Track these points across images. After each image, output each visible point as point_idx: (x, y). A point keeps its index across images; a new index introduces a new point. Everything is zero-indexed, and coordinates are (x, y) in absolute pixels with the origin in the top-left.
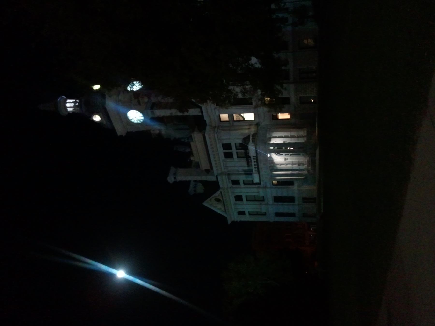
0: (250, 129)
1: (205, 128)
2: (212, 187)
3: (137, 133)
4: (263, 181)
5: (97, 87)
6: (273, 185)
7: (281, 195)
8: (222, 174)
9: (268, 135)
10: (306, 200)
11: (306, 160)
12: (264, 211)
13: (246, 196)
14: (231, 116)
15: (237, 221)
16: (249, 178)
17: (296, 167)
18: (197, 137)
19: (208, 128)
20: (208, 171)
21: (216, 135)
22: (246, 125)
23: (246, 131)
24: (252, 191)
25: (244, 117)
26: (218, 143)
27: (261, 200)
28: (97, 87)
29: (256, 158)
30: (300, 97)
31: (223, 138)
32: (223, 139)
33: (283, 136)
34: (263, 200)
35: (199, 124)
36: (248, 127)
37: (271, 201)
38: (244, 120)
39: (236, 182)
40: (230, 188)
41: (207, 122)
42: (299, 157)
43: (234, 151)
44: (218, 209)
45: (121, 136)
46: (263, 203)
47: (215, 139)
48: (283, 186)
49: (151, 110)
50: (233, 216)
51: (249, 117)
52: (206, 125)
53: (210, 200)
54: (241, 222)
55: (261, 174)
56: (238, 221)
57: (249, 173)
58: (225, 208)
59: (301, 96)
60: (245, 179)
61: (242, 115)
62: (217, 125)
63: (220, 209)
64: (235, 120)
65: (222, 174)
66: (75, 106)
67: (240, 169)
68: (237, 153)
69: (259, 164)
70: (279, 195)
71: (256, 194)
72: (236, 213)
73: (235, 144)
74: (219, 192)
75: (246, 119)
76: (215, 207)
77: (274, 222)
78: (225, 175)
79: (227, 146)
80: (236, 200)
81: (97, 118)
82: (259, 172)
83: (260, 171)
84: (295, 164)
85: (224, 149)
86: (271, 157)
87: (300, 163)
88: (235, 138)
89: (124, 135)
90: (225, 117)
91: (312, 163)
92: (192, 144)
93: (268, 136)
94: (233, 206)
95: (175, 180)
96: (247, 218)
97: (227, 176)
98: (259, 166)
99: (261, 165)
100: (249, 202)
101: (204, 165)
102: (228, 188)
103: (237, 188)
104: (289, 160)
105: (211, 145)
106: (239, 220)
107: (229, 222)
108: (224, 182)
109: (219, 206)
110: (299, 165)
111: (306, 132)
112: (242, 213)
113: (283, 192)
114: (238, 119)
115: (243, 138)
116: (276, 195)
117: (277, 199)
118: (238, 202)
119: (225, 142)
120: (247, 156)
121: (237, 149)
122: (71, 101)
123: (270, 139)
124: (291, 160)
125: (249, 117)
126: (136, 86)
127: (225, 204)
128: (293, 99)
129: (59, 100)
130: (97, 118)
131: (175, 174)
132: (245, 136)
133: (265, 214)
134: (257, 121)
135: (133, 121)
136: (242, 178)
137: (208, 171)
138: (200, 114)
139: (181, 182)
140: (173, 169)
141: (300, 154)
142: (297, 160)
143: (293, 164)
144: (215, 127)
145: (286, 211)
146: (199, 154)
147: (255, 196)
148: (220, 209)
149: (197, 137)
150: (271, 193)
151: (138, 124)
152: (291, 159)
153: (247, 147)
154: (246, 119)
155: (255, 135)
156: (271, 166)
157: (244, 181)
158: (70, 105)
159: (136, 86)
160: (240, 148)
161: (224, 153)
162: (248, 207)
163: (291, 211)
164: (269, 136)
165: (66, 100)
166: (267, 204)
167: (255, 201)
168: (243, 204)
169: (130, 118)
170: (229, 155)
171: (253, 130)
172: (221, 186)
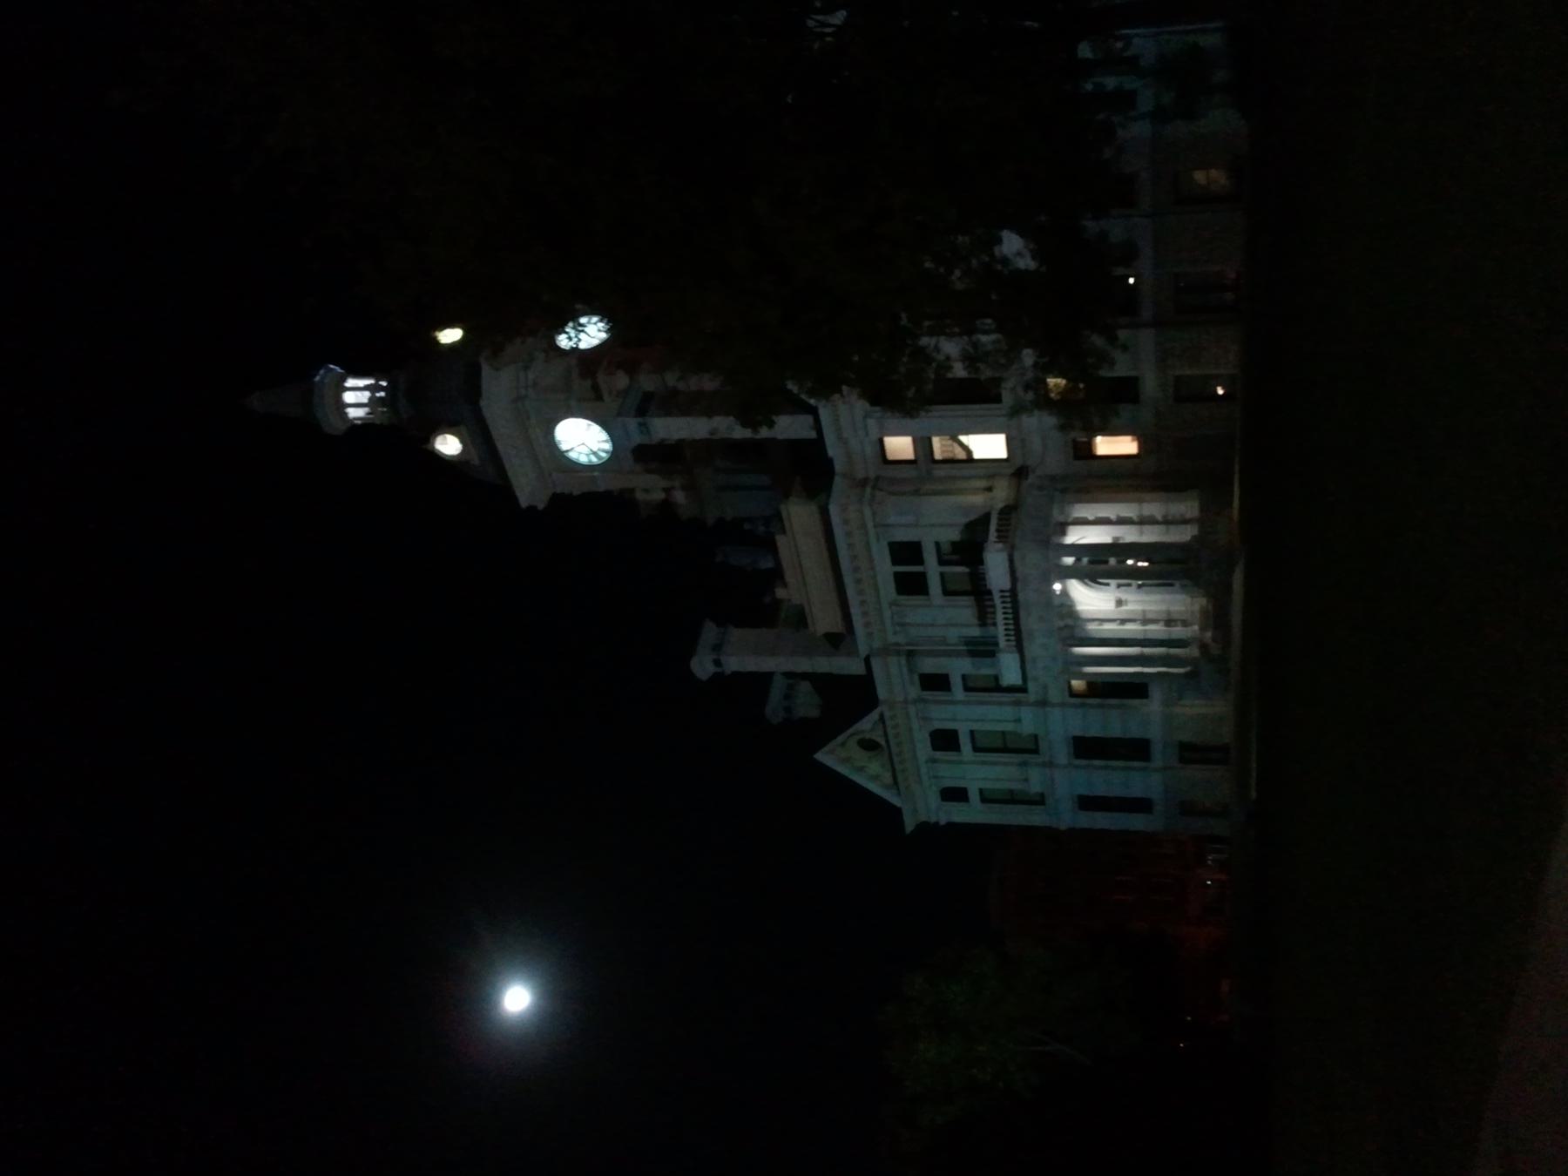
2: (851, 698)
3: (584, 502)
5: (450, 336)
9: (1055, 512)
10: (1190, 753)
11: (1197, 607)
12: (1035, 787)
13: (972, 732)
14: (923, 445)
15: (937, 823)
18: (799, 514)
19: (837, 480)
20: (838, 641)
21: (867, 512)
23: (978, 499)
24: (994, 716)
25: (972, 447)
26: (873, 540)
28: (450, 336)
31: (892, 520)
33: (1113, 517)
34: (1036, 751)
35: (809, 469)
36: (983, 484)
37: (1062, 755)
38: (970, 459)
39: (936, 683)
40: (915, 702)
41: (839, 467)
43: (932, 568)
44: (870, 775)
47: (864, 526)
50: (922, 806)
51: (989, 446)
53: (843, 744)
55: (1027, 653)
56: (943, 822)
57: (983, 649)
61: (963, 438)
62: (872, 475)
64: (938, 455)
66: (373, 402)
67: (953, 634)
68: (942, 575)
69: (1023, 621)
71: (1009, 727)
72: (934, 799)
74: (874, 715)
75: (976, 456)
76: (861, 769)
77: (1072, 832)
78: (898, 653)
79: (906, 552)
80: (935, 748)
81: (449, 445)
82: (1020, 648)
85: (895, 562)
86: (1065, 592)
87: (1175, 616)
88: (936, 522)
90: (900, 446)
91: (1217, 618)
92: (781, 541)
96: (972, 813)
97: (903, 661)
99: (1030, 622)
101: (824, 620)
102: (906, 701)
105: (849, 534)
107: (909, 825)
108: (892, 682)
110: (1169, 622)
112: (955, 795)
116: (1078, 733)
117: (1086, 748)
120: (978, 591)
121: (942, 562)
122: (362, 383)
123: (1062, 529)
125: (989, 446)
126: (591, 333)
128: (1150, 385)
129: (317, 378)
130: (449, 445)
131: (717, 648)
132: (973, 517)
134: (1018, 462)
135: (573, 455)
136: (958, 667)
137: (838, 641)
139: (736, 674)
140: (710, 632)
142: (1163, 607)
143: (1146, 621)
144: (863, 483)
145: (1117, 791)
147: (1003, 733)
148: (875, 778)
149: (799, 514)
150: (1062, 725)
151: (590, 468)
155: (1008, 511)
157: (964, 677)
159: (591, 333)
160: (954, 557)
162: (977, 773)
164: (1061, 519)
166: (1050, 764)
169: (564, 447)
170: (911, 585)
171: (1002, 493)
172: (882, 693)
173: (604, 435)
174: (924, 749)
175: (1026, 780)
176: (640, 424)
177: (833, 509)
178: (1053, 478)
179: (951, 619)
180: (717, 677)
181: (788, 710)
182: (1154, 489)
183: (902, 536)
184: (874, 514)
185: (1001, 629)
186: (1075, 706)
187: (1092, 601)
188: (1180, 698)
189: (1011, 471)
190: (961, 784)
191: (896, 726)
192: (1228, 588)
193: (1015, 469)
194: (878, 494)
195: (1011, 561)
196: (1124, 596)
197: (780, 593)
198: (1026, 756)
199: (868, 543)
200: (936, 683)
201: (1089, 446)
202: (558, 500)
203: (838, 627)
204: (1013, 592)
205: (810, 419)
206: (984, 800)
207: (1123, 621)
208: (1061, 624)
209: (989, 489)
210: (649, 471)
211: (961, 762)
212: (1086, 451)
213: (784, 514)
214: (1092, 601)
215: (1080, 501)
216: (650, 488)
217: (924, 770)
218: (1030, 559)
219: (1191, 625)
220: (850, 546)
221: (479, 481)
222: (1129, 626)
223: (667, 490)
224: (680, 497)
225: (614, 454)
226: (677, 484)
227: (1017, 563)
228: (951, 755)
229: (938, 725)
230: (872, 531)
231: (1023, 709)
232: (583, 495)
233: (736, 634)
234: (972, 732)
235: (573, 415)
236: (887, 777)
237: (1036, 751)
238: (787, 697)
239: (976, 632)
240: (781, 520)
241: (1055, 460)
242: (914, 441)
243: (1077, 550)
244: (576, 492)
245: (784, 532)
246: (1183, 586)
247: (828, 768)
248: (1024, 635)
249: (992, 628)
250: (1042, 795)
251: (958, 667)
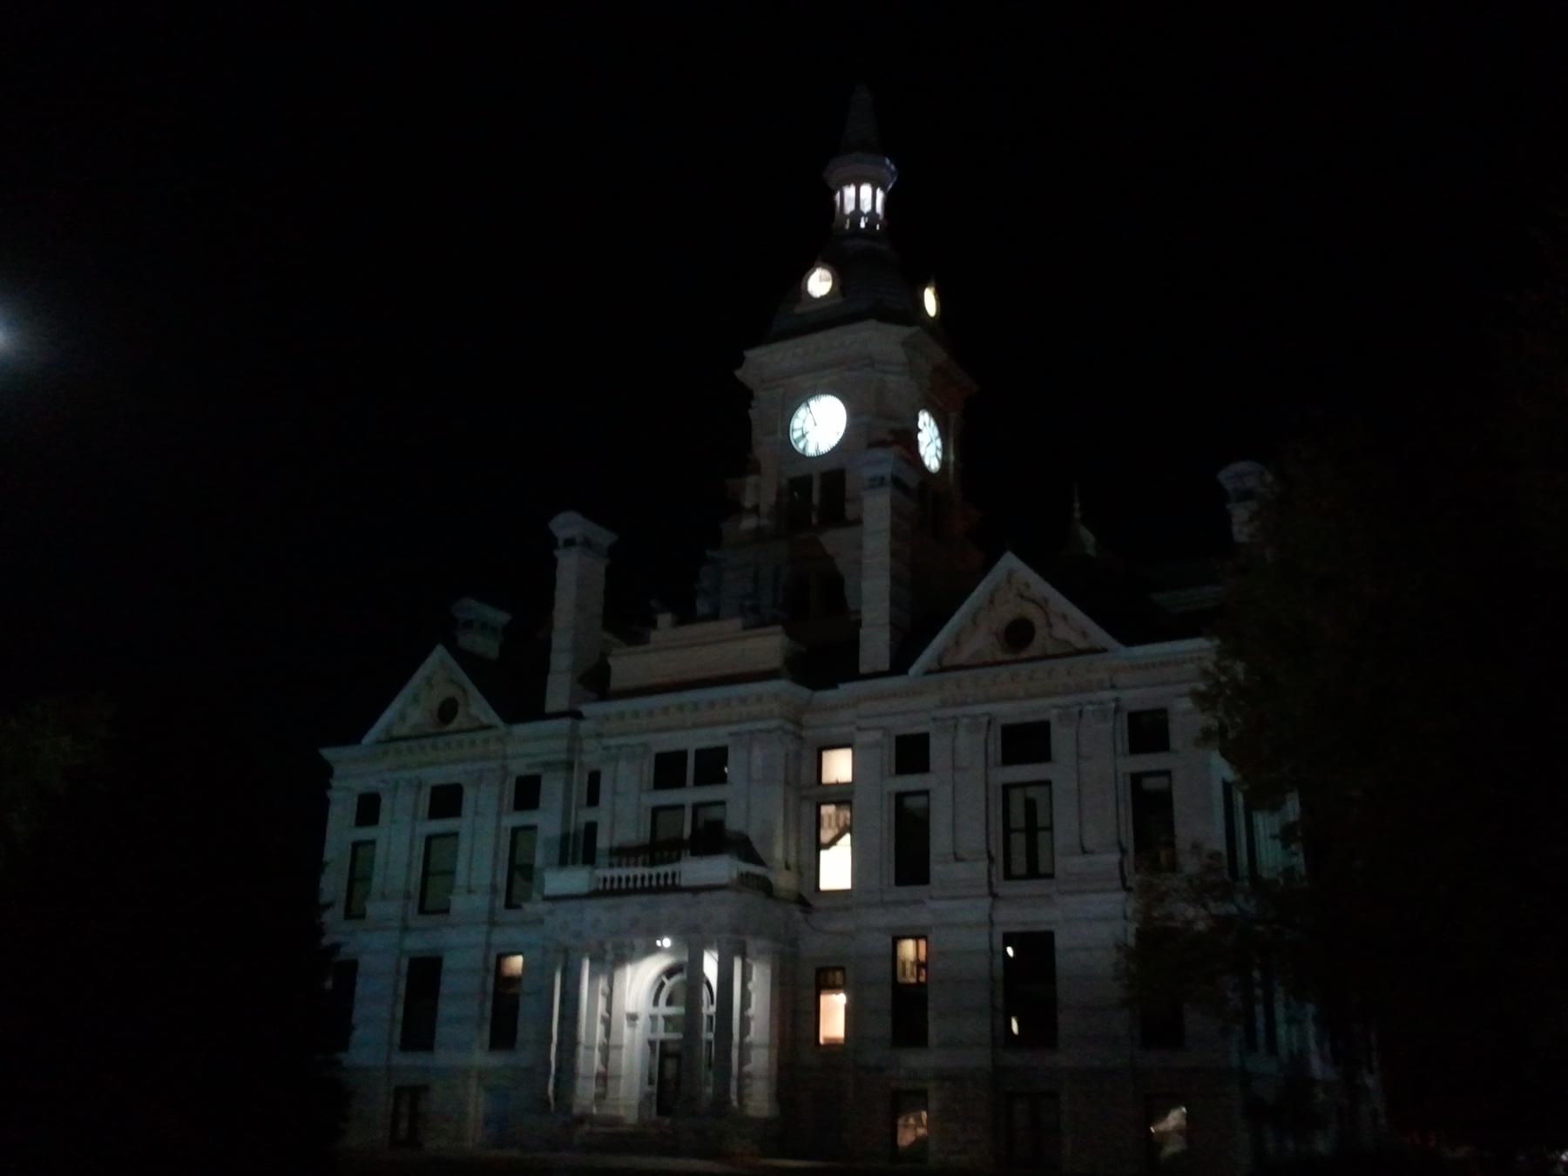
0: (788, 867)
2: (516, 691)
3: (738, 426)
6: (501, 957)
9: (762, 943)
10: (411, 1096)
11: (622, 1112)
14: (841, 795)
17: (589, 1061)
18: (769, 646)
19: (805, 692)
20: (596, 682)
21: (773, 723)
23: (778, 853)
25: (833, 849)
26: (734, 728)
31: (757, 754)
32: (750, 753)
35: (824, 659)
37: (417, 943)
38: (819, 846)
39: (527, 794)
40: (504, 768)
41: (828, 696)
42: (636, 1080)
43: (688, 796)
44: (407, 709)
45: (739, 361)
46: (413, 906)
48: (489, 1004)
49: (888, 478)
50: (352, 771)
51: (836, 869)
54: (324, 804)
55: (592, 902)
57: (579, 847)
58: (406, 738)
61: (847, 839)
63: (402, 717)
65: (574, 737)
67: (601, 815)
68: (681, 807)
69: (634, 899)
71: (461, 878)
72: (361, 786)
73: (722, 803)
75: (823, 853)
76: (416, 699)
78: (570, 750)
79: (712, 766)
80: (436, 790)
81: (819, 283)
82: (594, 894)
84: (605, 1060)
85: (700, 753)
86: (652, 950)
87: (611, 1084)
88: (748, 801)
89: (738, 373)
90: (839, 766)
93: (753, 945)
95: (561, 543)
96: (340, 829)
97: (563, 756)
99: (632, 907)
101: (627, 666)
102: (505, 757)
103: (501, 798)
104: (626, 1030)
105: (621, 715)
106: (333, 795)
107: (328, 753)
108: (531, 743)
110: (603, 1078)
112: (368, 810)
115: (752, 839)
116: (360, 969)
117: (424, 977)
118: (996, 734)
119: (469, 794)
120: (660, 849)
121: (696, 807)
125: (836, 869)
126: (930, 445)
127: (427, 742)
128: (914, 1060)
129: (888, 161)
130: (819, 283)
131: (587, 544)
134: (817, 903)
135: (802, 413)
136: (547, 821)
137: (596, 682)
138: (863, 669)
139: (553, 563)
140: (605, 538)
141: (651, 1082)
142: (624, 1071)
143: (606, 1049)
144: (798, 723)
146: (670, 648)
147: (451, 872)
148: (402, 717)
150: (460, 949)
151: (786, 430)
152: (633, 1044)
155: (765, 887)
157: (533, 828)
159: (930, 445)
160: (701, 824)
161: (683, 755)
162: (398, 842)
165: (884, 189)
166: (406, 929)
168: (499, 814)
169: (812, 403)
170: (668, 770)
171: (784, 881)
172: (522, 729)
173: (825, 448)
175: (470, 891)
176: (882, 479)
179: (625, 814)
180: (551, 542)
181: (469, 624)
184: (769, 731)
185: (608, 873)
186: (486, 960)
190: (384, 817)
191: (486, 741)
192: (674, 1152)
193: (808, 897)
195: (989, 871)
196: (640, 1023)
197: (664, 619)
198: (416, 900)
201: (834, 988)
203: (616, 683)
204: (676, 889)
207: (607, 1023)
208: (609, 947)
209: (788, 867)
210: (779, 494)
211: (415, 817)
213: (770, 629)
214: (639, 983)
217: (407, 774)
218: (721, 910)
220: (636, 714)
221: (776, 310)
223: (756, 510)
224: (748, 523)
225: (802, 457)
226: (765, 522)
232: (746, 425)
233: (600, 567)
234: (455, 834)
238: (484, 625)
239: (602, 842)
241: (817, 945)
242: (846, 784)
243: (697, 963)
244: (753, 414)
245: (745, 628)
246: (648, 1096)
250: (362, 916)
251: (547, 821)
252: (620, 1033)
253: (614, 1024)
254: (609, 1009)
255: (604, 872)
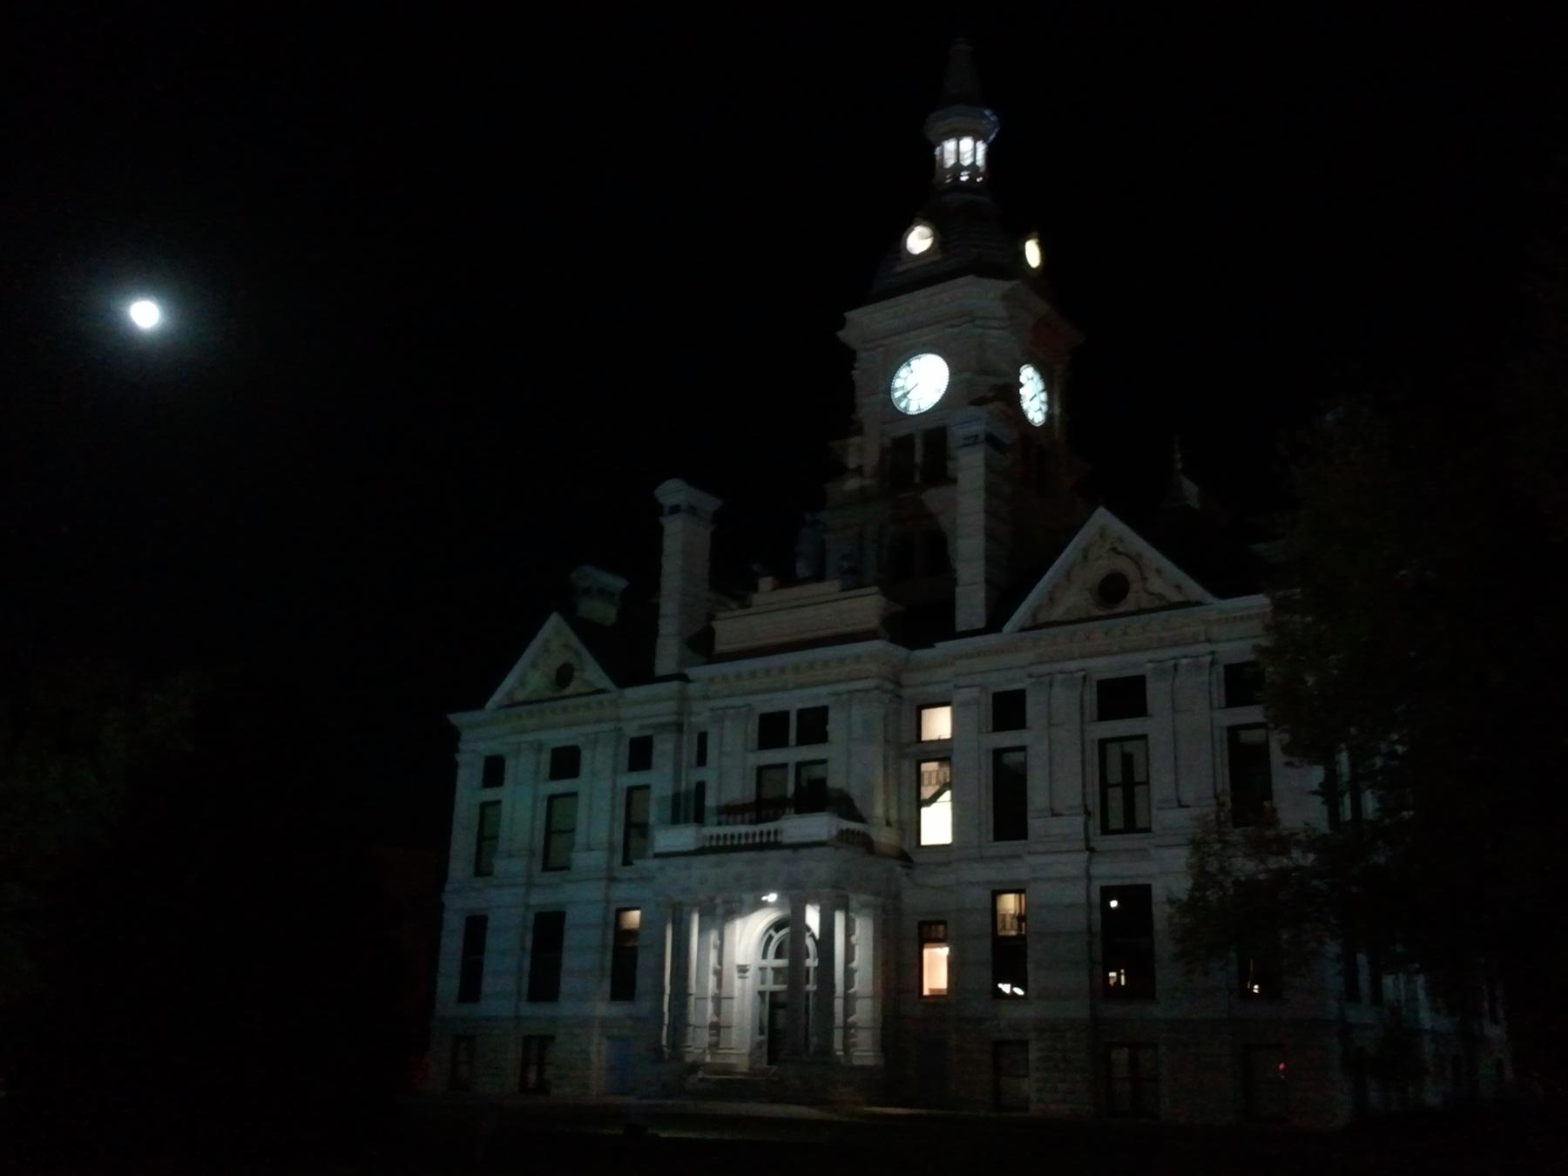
0: (888, 824)
1: (894, 640)
2: (628, 658)
3: (842, 386)
4: (662, 869)
5: (1033, 254)
7: (567, 942)
8: (684, 699)
9: (864, 898)
10: (537, 1047)
11: (733, 1060)
12: (500, 865)
13: (498, 802)
14: (940, 751)
15: (457, 750)
16: (655, 812)
18: (867, 606)
19: (902, 652)
20: (702, 645)
21: (871, 683)
22: (899, 810)
23: (879, 811)
24: (596, 821)
25: (934, 805)
27: (553, 854)
28: (1033, 254)
29: (772, 845)
30: (1024, 1044)
33: (854, 964)
34: (546, 868)
35: (921, 619)
36: (894, 816)
37: (541, 899)
38: (921, 803)
39: (640, 754)
43: (791, 755)
44: (526, 675)
45: (842, 323)
47: (851, 679)
48: (609, 956)
49: (982, 437)
50: (478, 734)
51: (937, 825)
52: (913, 648)
53: (567, 646)
54: (453, 767)
55: (697, 861)
56: (460, 758)
57: (688, 807)
59: (1032, 1046)
60: (656, 793)
61: (947, 795)
62: (906, 693)
64: (925, 767)
65: (684, 699)
66: (958, 167)
67: (708, 775)
68: (784, 766)
70: (571, 938)
71: (580, 838)
72: (494, 748)
74: (605, 682)
75: (924, 811)
76: (534, 665)
77: (441, 907)
78: (680, 714)
79: (814, 726)
81: (919, 240)
82: (700, 852)
83: (713, 858)
85: (802, 713)
86: (760, 905)
88: (849, 759)
91: (729, 1085)
92: (831, 587)
94: (530, 737)
95: (666, 510)
96: (468, 793)
98: (735, 855)
99: (737, 864)
100: (621, 799)
101: (731, 630)
104: (737, 983)
105: (842, 661)
106: (461, 758)
107: (456, 718)
108: (643, 706)
109: (1075, 599)
110: (716, 1027)
111: (870, 1062)
112: (494, 772)
113: (582, 956)
114: (925, 780)
116: (491, 924)
117: (549, 930)
118: (546, 758)
120: (764, 807)
121: (800, 766)
122: (980, 161)
123: (846, 909)
124: (737, 993)
125: (937, 825)
130: (919, 240)
131: (692, 510)
132: (858, 804)
133: (482, 868)
134: (918, 859)
136: (660, 781)
137: (702, 645)
139: (661, 529)
140: (710, 504)
141: (761, 1032)
142: (735, 1019)
143: (718, 1000)
144: (899, 684)
145: (491, 962)
146: (774, 611)
147: (572, 831)
148: (522, 682)
149: (867, 606)
150: (581, 900)
151: (889, 390)
152: (743, 997)
153: (799, 805)
154: (926, 812)
155: (866, 844)
156: (715, 907)
157: (647, 787)
158: (964, 152)
162: (521, 803)
163: (489, 984)
164: (854, 904)
165: (985, 141)
166: (530, 885)
167: (549, 832)
168: (615, 771)
169: (915, 362)
170: (772, 730)
171: (885, 837)
172: (631, 693)
174: (562, 737)
175: (510, 855)
176: (976, 436)
177: (877, 645)
178: (897, 897)
179: (731, 773)
180: (657, 509)
182: (885, 1018)
183: (835, 726)
187: (748, 936)
188: (609, 1038)
189: (906, 848)
193: (910, 853)
194: (887, 697)
197: (766, 583)
199: (1147, 649)
200: (640, 754)
201: (938, 941)
202: (847, 356)
203: (720, 647)
204: (777, 846)
205: (981, 624)
206: (484, 806)
207: (719, 974)
209: (888, 824)
212: (928, 936)
214: (748, 936)
215: (875, 931)
216: (863, 453)
218: (820, 866)
219: (713, 1054)
221: (875, 271)
222: (712, 981)
223: (859, 471)
224: (852, 484)
225: (904, 416)
227: (818, 851)
228: (546, 768)
229: (586, 755)
230: (842, 687)
231: (1080, 820)
235: (952, 374)
236: (520, 696)
237: (546, 868)
239: (710, 801)
240: (860, 586)
241: (917, 900)
247: (1064, 547)
248: (724, 857)
249: (715, 820)
250: (490, 874)
252: (731, 985)
253: (725, 972)
254: (720, 962)
255: (711, 830)
